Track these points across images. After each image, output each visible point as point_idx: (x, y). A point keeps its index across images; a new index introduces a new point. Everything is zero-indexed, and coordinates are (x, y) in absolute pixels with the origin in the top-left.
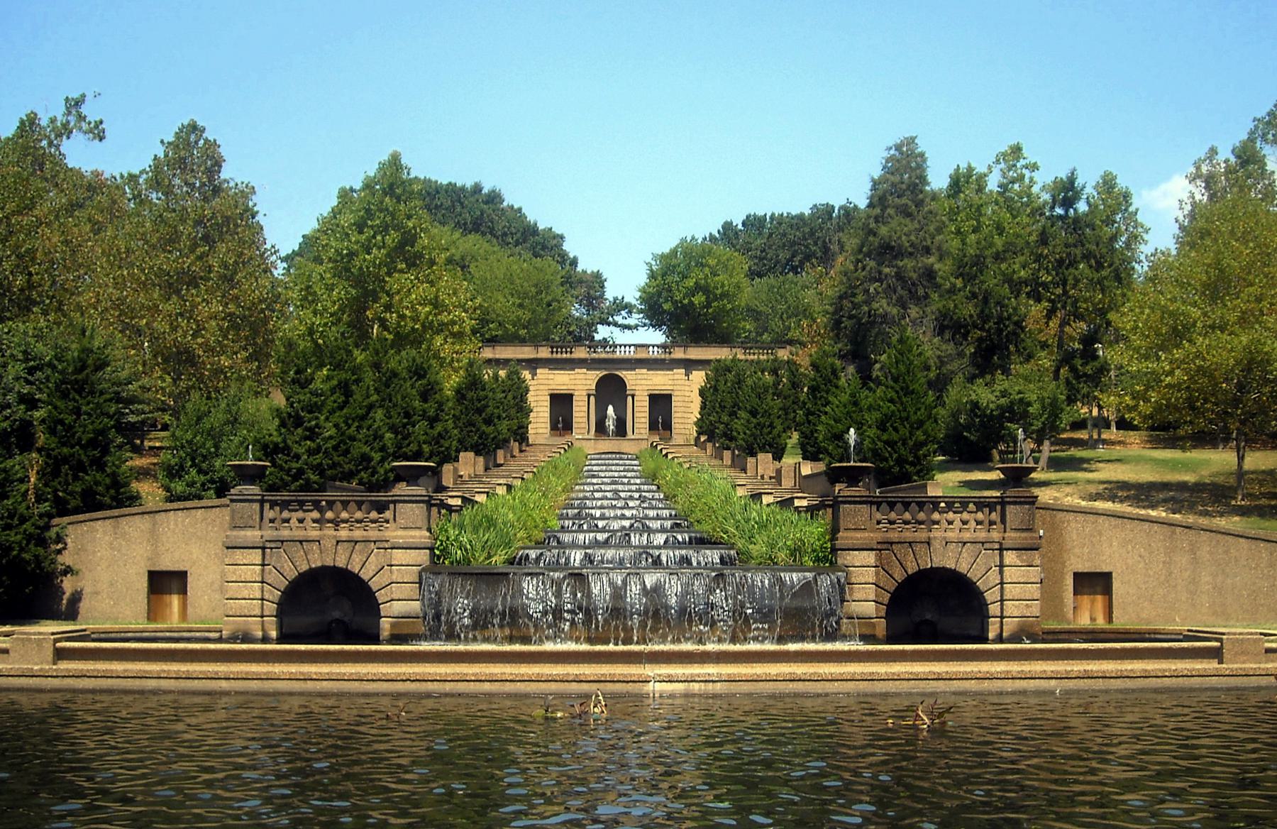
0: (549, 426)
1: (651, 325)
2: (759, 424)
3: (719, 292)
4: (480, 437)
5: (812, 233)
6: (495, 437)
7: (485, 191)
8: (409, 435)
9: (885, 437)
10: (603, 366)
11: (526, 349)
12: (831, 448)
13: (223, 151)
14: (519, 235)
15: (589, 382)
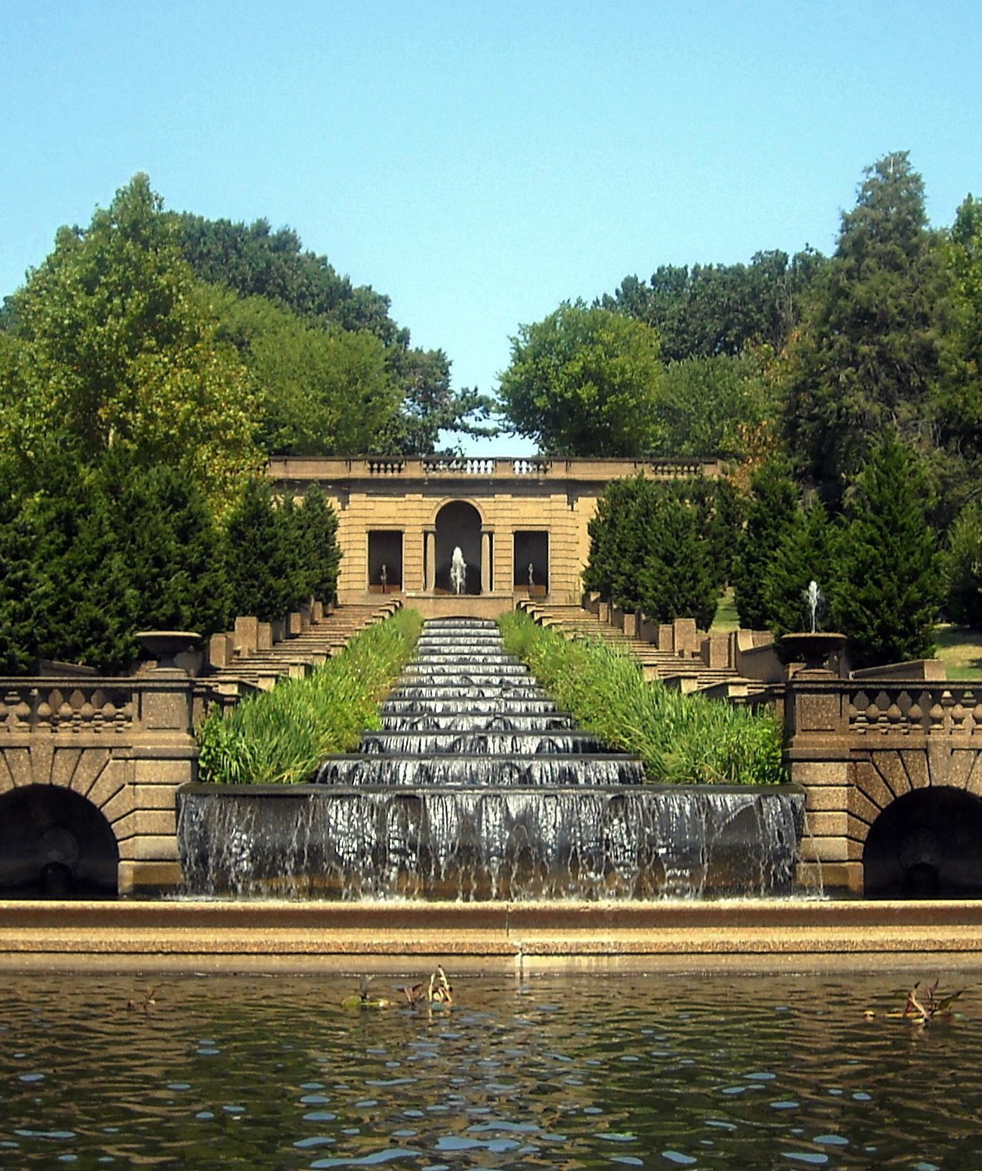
0: (367, 578)
1: (518, 429)
2: (676, 575)
3: (617, 380)
4: (266, 595)
5: (754, 295)
6: (288, 595)
7: (273, 232)
11: (334, 465)
14: (322, 297)
15: (425, 514)
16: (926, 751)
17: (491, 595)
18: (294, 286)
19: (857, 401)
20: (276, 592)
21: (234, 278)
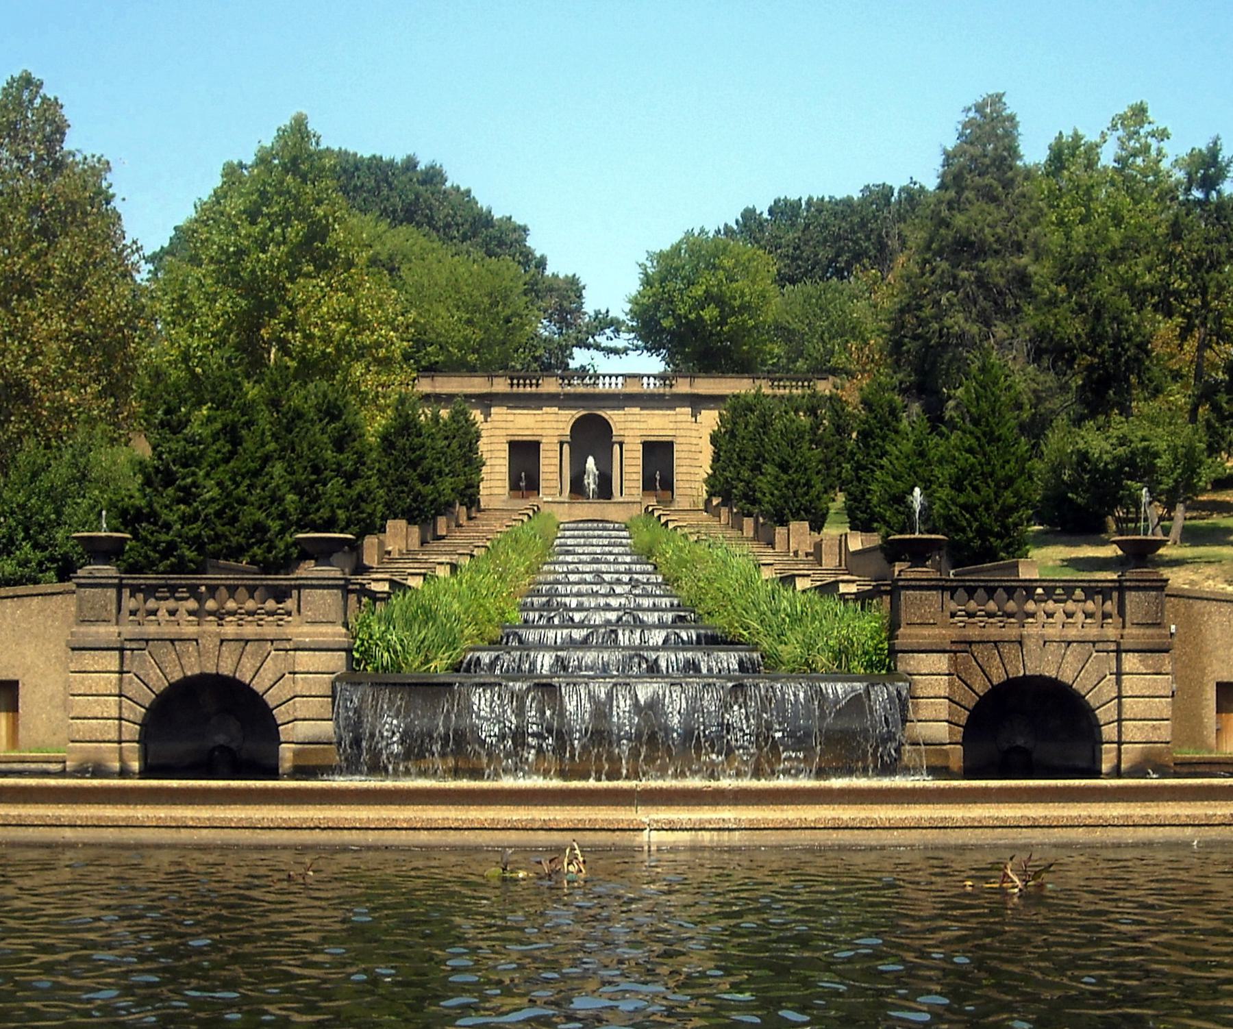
1: (646, 348)
2: (791, 482)
3: (737, 303)
4: (414, 500)
5: (863, 224)
6: (435, 500)
8: (318, 496)
9: (962, 499)
10: (580, 403)
11: (477, 380)
12: (888, 514)
13: (68, 113)
14: (467, 226)
15: (561, 425)
16: (1020, 643)
17: (621, 500)
18: (440, 216)
19: (958, 321)
20: (424, 497)
21: (385, 209)
